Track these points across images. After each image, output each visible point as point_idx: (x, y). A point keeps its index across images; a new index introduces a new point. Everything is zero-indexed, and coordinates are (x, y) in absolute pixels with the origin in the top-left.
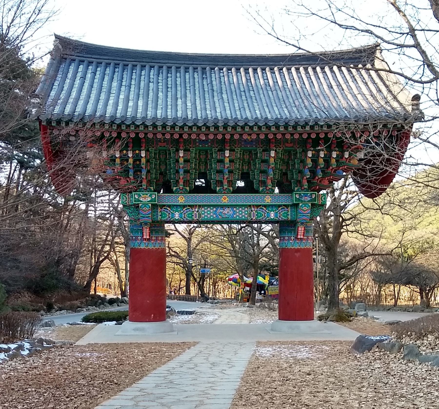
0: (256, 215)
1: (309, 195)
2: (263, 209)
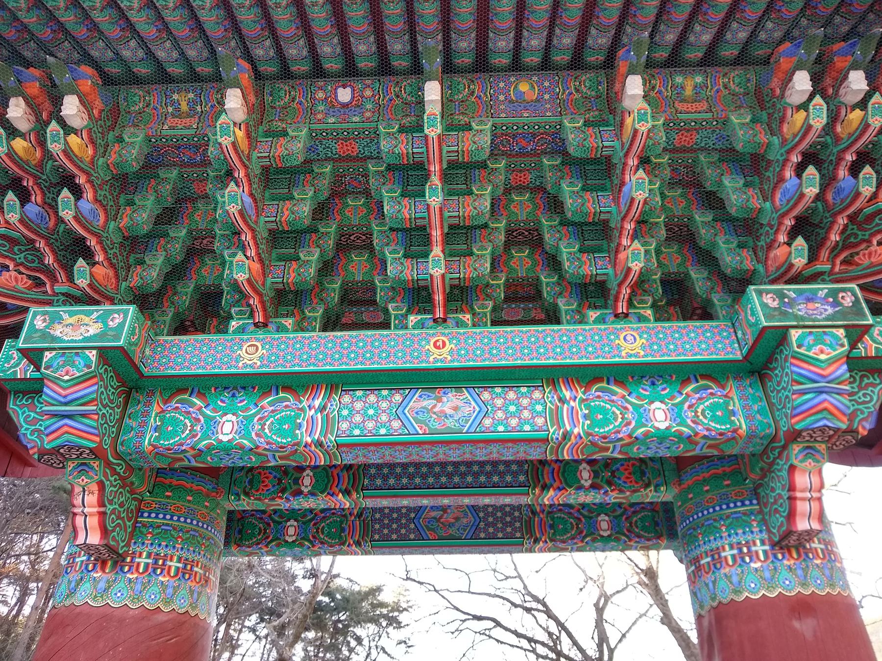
0: (586, 417)
1: (821, 294)
2: (614, 393)
